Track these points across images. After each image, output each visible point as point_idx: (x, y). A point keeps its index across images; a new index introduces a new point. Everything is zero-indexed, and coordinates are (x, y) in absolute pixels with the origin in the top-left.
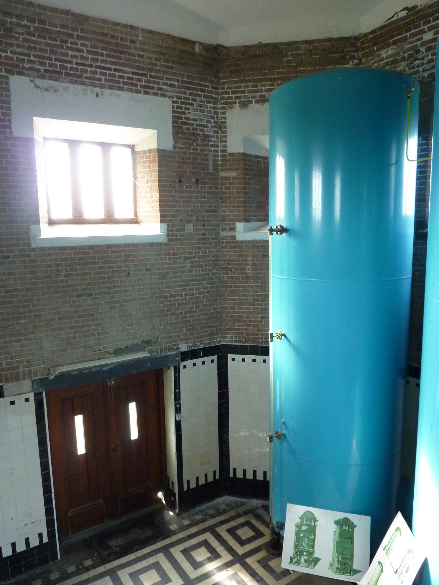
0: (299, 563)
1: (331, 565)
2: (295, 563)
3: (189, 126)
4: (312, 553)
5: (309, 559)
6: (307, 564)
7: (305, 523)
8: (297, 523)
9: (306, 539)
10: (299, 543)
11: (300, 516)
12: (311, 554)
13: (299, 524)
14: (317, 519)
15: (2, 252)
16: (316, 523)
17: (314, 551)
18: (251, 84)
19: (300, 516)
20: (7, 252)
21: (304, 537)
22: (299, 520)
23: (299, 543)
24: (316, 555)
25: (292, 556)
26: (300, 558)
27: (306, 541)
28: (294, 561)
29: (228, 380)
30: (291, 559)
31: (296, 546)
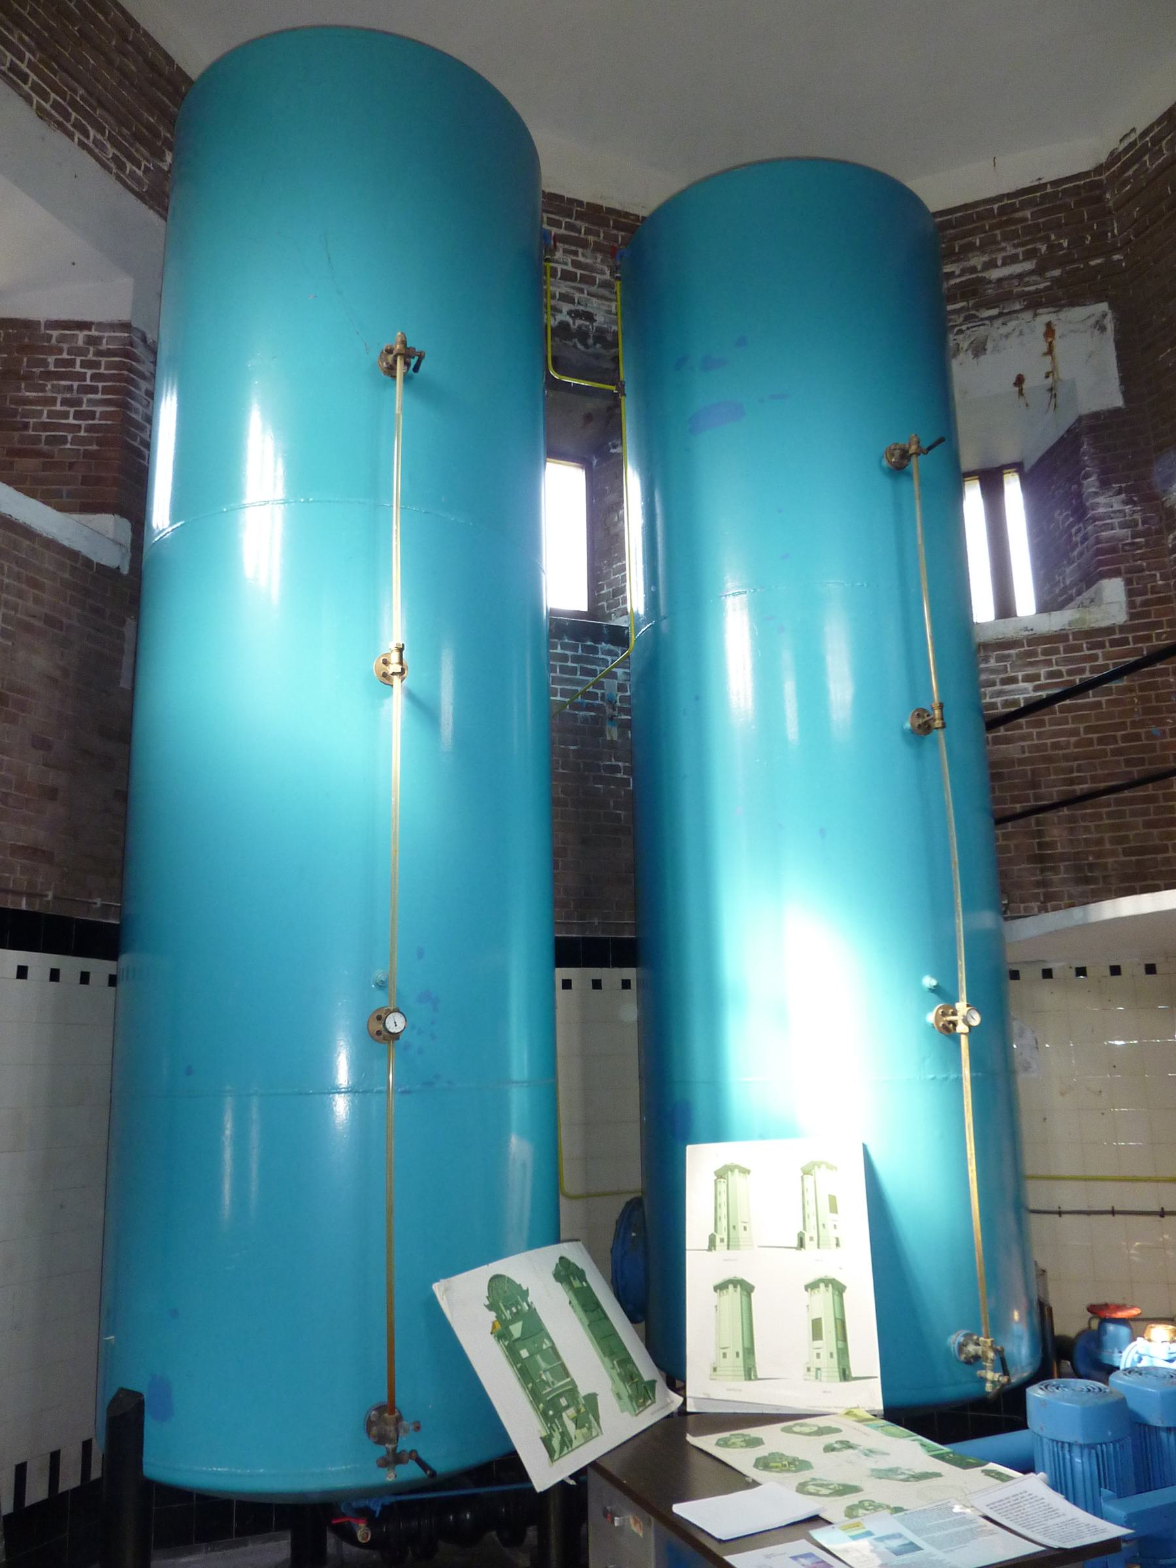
0: (571, 1441)
1: (420, 954)
2: (561, 1450)
3: (69, 383)
4: (570, 1390)
5: (578, 1411)
6: (584, 1430)
7: (509, 1317)
8: (494, 1327)
9: (538, 1357)
10: (533, 1382)
11: (487, 1303)
12: (572, 1391)
13: (498, 1326)
14: (525, 1288)
15: (1170, 624)
16: (529, 1299)
17: (572, 1380)
18: (619, 775)
19: (487, 1303)
20: (79, 426)
21: (532, 1355)
22: (493, 1314)
23: (533, 1382)
24: (583, 1391)
25: (544, 1434)
26: (563, 1425)
27: (543, 1365)
28: (556, 1443)
29: (9, 948)
30: (547, 1441)
31: (535, 1396)
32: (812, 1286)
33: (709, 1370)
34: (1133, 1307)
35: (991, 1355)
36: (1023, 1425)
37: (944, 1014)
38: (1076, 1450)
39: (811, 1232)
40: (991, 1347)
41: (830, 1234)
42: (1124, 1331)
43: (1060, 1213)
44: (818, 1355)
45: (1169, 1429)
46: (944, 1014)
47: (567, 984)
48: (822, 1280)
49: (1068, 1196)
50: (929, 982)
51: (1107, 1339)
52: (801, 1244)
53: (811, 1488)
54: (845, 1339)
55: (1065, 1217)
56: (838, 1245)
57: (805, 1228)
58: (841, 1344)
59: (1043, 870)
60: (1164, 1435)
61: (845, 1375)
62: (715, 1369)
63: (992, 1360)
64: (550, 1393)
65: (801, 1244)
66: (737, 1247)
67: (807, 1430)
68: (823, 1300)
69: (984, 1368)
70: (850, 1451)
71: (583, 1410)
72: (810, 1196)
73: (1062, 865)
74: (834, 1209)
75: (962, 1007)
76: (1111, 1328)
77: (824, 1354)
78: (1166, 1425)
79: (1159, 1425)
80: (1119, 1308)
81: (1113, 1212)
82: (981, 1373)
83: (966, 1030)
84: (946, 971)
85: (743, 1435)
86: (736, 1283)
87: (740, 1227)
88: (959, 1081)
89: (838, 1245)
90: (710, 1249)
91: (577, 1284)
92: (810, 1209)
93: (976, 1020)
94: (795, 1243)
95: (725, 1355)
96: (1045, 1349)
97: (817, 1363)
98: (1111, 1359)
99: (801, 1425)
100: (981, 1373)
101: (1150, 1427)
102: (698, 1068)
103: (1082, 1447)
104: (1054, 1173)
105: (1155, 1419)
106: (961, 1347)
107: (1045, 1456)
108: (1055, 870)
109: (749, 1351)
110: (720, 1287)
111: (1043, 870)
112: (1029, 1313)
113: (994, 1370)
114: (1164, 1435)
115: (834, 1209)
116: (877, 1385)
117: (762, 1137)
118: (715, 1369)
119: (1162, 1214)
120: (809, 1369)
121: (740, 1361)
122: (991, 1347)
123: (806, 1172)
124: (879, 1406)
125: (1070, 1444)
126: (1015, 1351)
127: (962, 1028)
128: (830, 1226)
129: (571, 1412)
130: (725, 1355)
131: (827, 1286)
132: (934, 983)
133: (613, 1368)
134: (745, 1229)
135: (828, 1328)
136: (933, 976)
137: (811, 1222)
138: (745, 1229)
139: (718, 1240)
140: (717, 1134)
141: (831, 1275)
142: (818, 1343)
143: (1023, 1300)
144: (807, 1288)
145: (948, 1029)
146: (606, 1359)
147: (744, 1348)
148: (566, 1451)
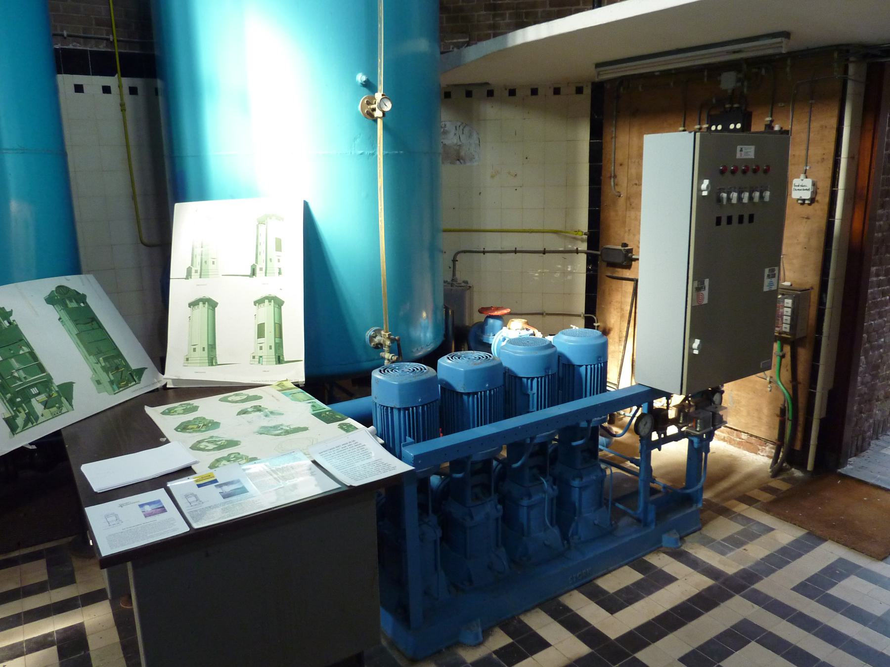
0: (37, 418)
2: (25, 425)
5: (50, 396)
12: (46, 384)
24: (58, 380)
25: (8, 415)
26: (31, 408)
28: (20, 421)
32: (259, 302)
33: (183, 360)
34: (505, 309)
35: (388, 343)
36: (369, 394)
37: (369, 103)
38: (396, 412)
39: (261, 264)
40: (389, 338)
41: (274, 266)
42: (498, 323)
43: (484, 252)
44: (261, 348)
45: (468, 394)
46: (369, 103)
47: (106, 90)
48: (266, 298)
49: (491, 242)
50: (361, 78)
51: (487, 328)
52: (253, 273)
53: (202, 445)
54: (281, 337)
55: (487, 254)
56: (280, 273)
57: (257, 262)
58: (277, 340)
59: (494, 16)
60: (465, 397)
61: (279, 360)
62: (187, 359)
63: (389, 346)
64: (20, 385)
65: (253, 273)
66: (207, 276)
67: (238, 398)
68: (266, 313)
69: (383, 351)
70: (258, 413)
71: (55, 395)
72: (262, 240)
73: (508, 12)
74: (279, 248)
75: (378, 96)
76: (491, 321)
77: (265, 347)
78: (467, 391)
79: (462, 391)
80: (497, 309)
81: (516, 252)
82: (382, 354)
83: (381, 115)
84: (371, 70)
85: (189, 404)
86: (204, 301)
87: (210, 262)
88: (374, 154)
89: (280, 273)
90: (187, 278)
91: (73, 305)
92: (262, 248)
93: (388, 106)
94: (249, 272)
95: (194, 350)
96: (446, 335)
97: (260, 353)
98: (488, 339)
99: (236, 395)
100: (382, 354)
101: (458, 393)
102: (188, 148)
103: (399, 409)
104: (482, 228)
105: (460, 388)
106: (372, 338)
107: (377, 417)
108: (503, 16)
109: (212, 347)
110: (193, 304)
111: (494, 16)
112: (435, 312)
113: (390, 353)
114: (465, 397)
115: (279, 248)
116: (302, 365)
117: (232, 197)
118: (187, 359)
119: (544, 252)
120: (254, 357)
121: (205, 354)
122: (389, 338)
123: (261, 222)
124: (302, 379)
125: (392, 409)
126: (422, 335)
127: (378, 114)
128: (275, 260)
129: (43, 397)
130: (194, 350)
131: (270, 302)
132: (364, 78)
133: (98, 362)
134: (213, 263)
135: (269, 330)
136: (365, 74)
137: (262, 257)
138: (213, 263)
139: (193, 271)
140: (202, 195)
141: (273, 294)
142: (261, 340)
143: (430, 306)
144: (255, 303)
145: (370, 114)
146: (92, 359)
147: (208, 345)
148: (30, 425)
